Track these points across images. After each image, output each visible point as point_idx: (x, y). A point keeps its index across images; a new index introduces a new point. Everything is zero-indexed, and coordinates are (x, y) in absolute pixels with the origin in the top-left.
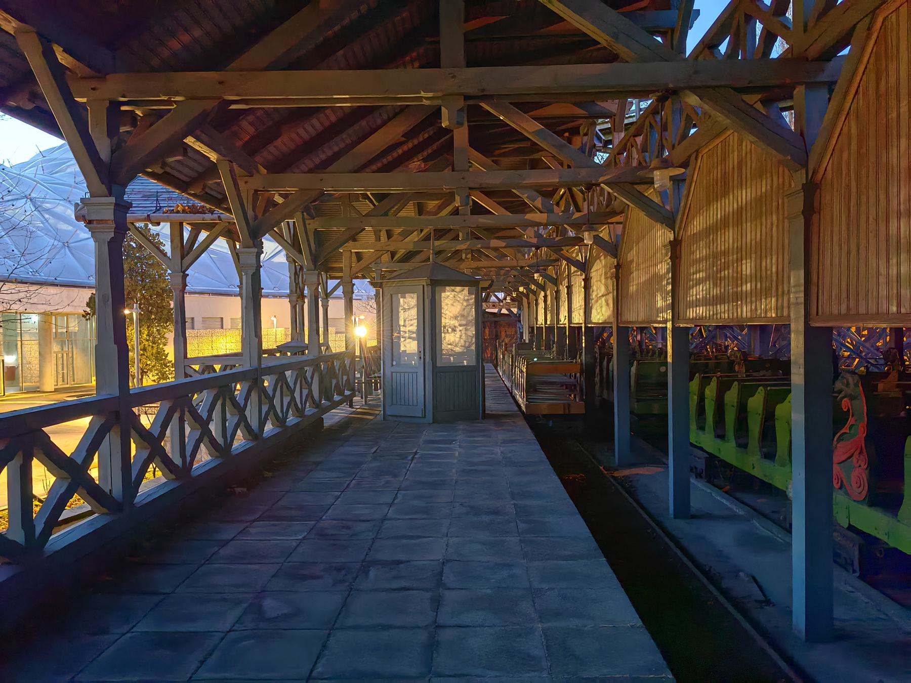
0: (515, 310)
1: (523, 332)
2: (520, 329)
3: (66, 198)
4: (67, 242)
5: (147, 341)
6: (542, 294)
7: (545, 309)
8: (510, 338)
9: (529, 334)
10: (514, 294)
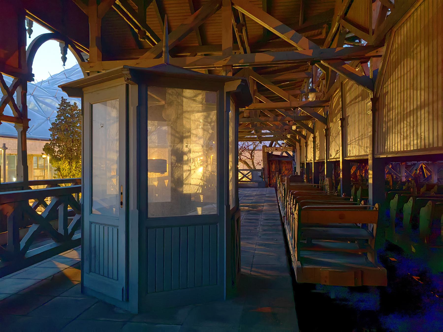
0: (291, 153)
1: (296, 167)
2: (294, 165)
3: (54, 96)
4: (49, 118)
5: (75, 170)
6: (312, 135)
7: (314, 148)
8: (288, 171)
9: (300, 168)
10: (289, 136)
